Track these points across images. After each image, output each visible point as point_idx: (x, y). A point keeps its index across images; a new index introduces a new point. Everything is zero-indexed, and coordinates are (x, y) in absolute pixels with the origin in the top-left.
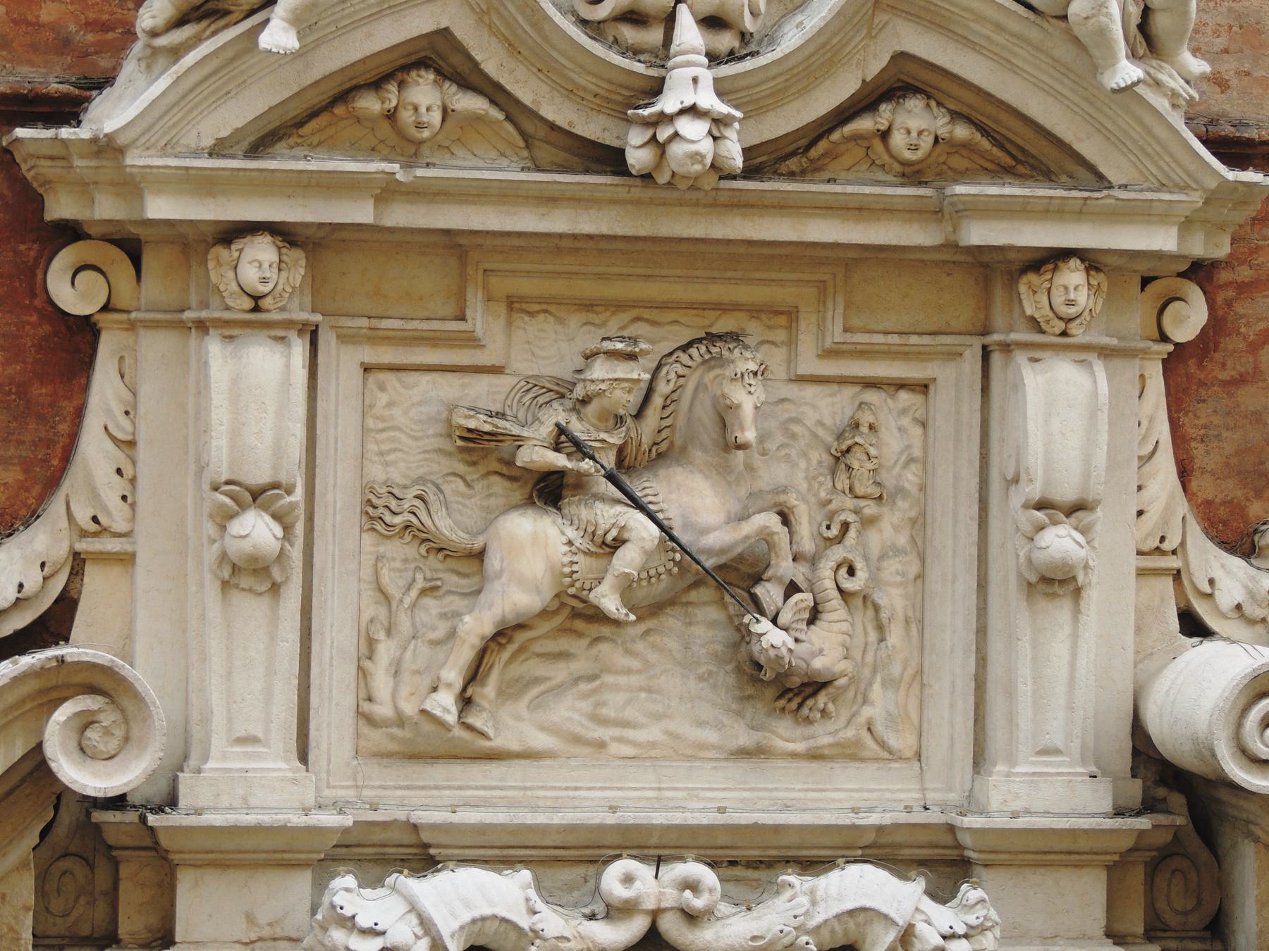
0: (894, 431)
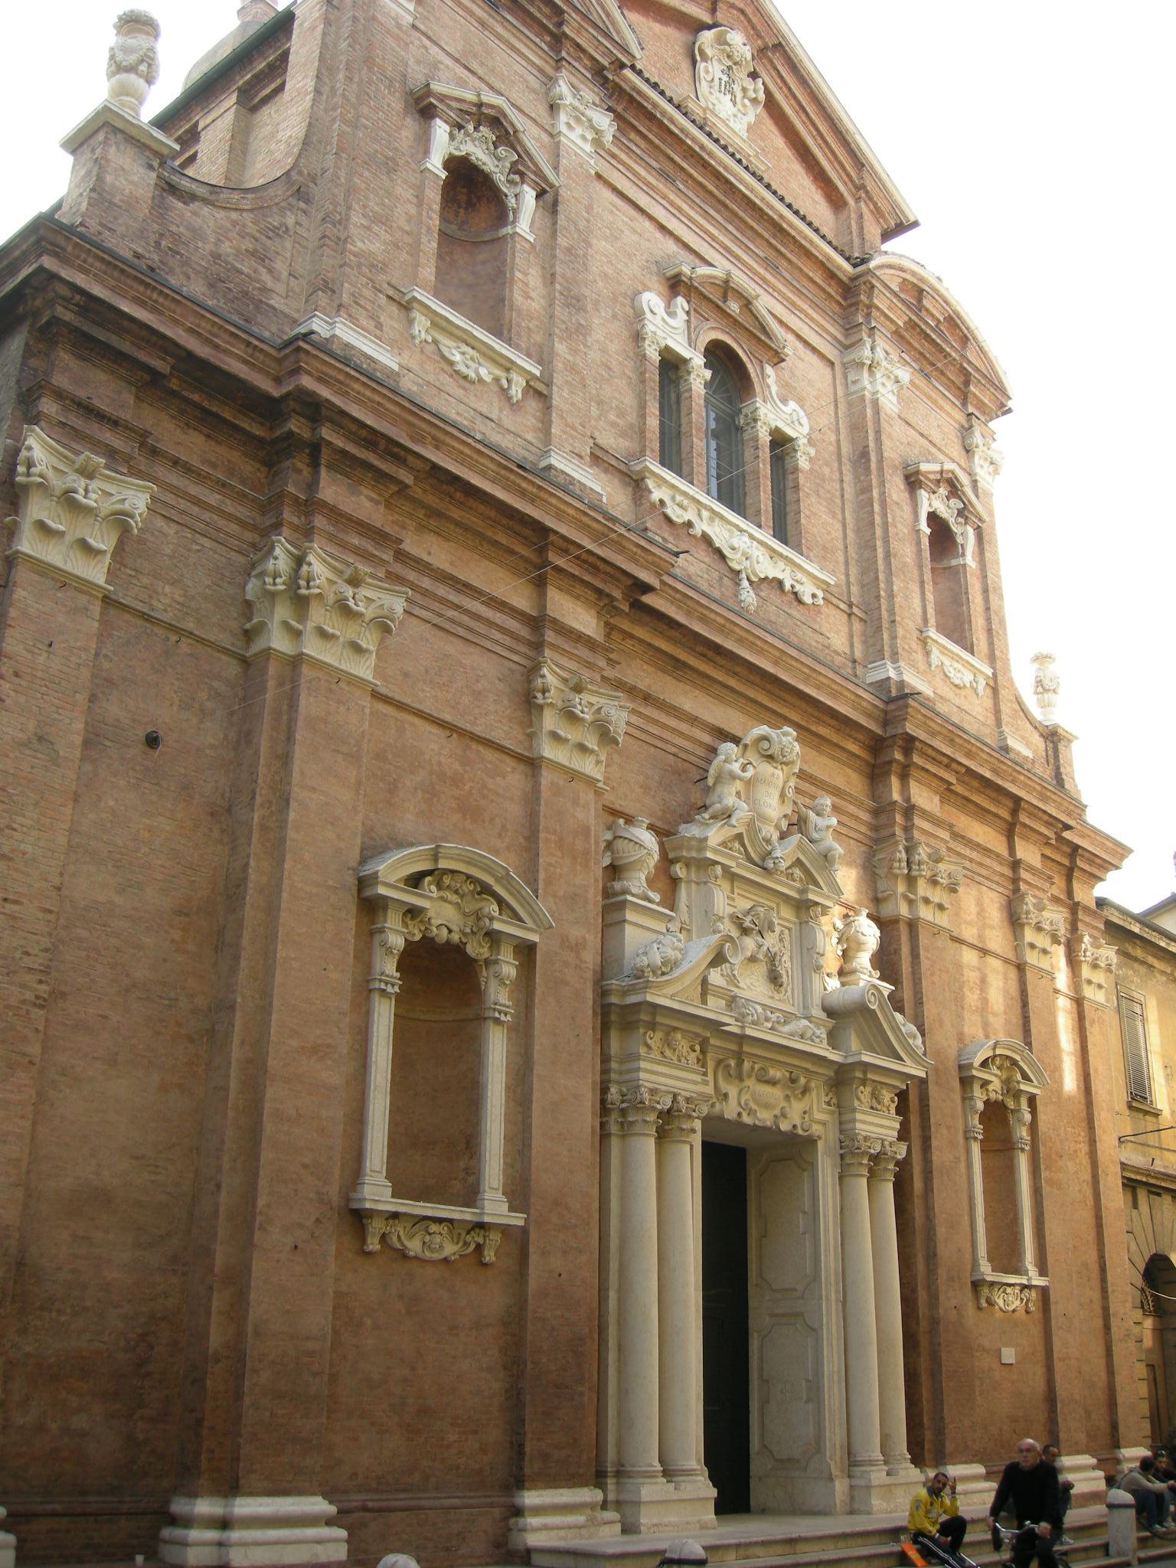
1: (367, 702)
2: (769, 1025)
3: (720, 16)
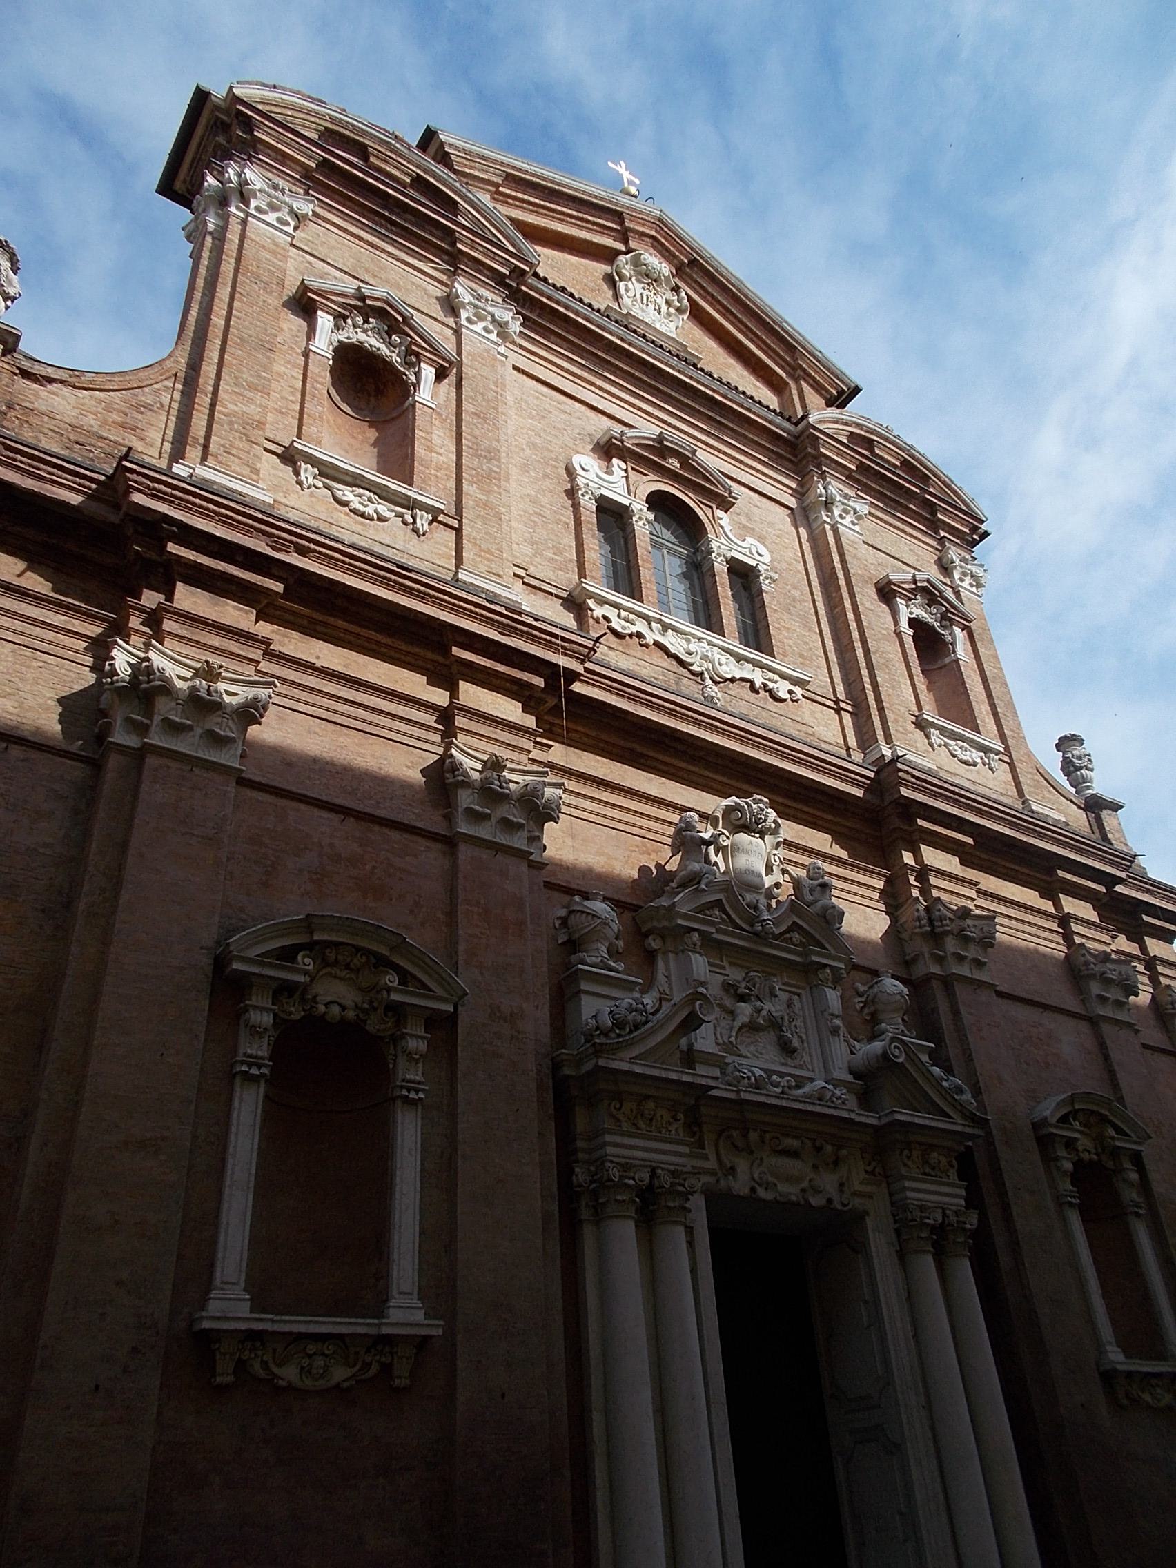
1: (231, 788)
2: (779, 1090)
3: (632, 244)
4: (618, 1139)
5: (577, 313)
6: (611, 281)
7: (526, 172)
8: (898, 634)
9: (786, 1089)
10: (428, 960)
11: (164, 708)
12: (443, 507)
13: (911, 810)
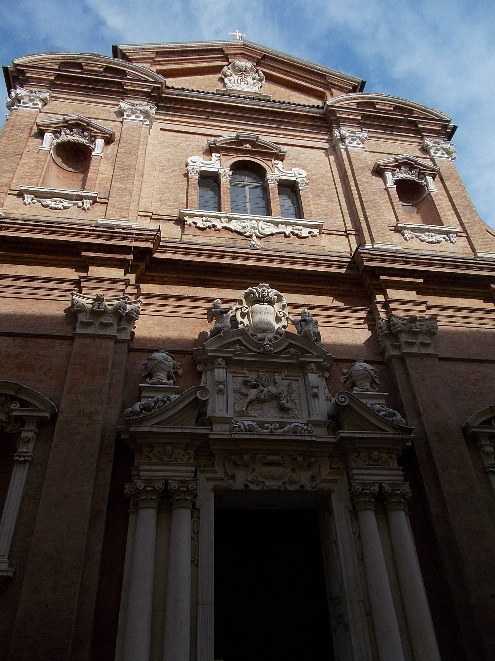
0: (294, 385)
3: (230, 60)
4: (148, 467)
5: (193, 97)
6: (222, 80)
7: (167, 48)
8: (387, 189)
9: (273, 430)
10: (35, 394)
11: (82, 318)
12: (458, 230)
13: (375, 272)
